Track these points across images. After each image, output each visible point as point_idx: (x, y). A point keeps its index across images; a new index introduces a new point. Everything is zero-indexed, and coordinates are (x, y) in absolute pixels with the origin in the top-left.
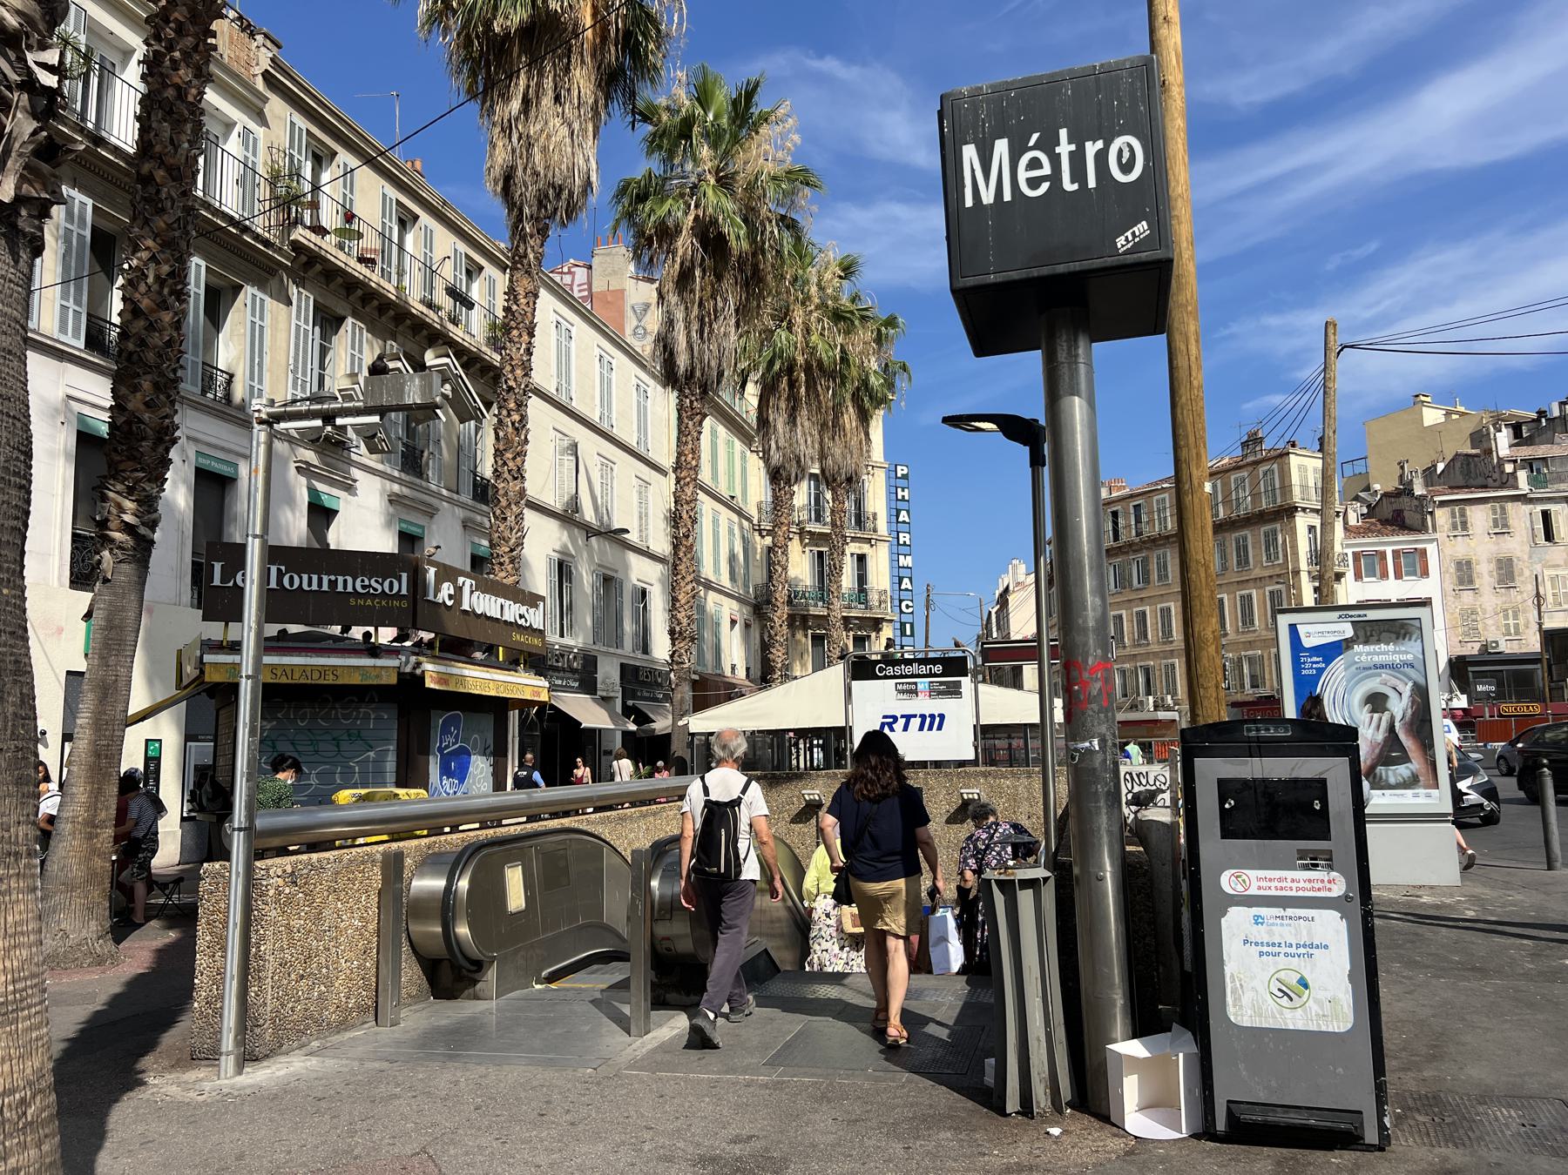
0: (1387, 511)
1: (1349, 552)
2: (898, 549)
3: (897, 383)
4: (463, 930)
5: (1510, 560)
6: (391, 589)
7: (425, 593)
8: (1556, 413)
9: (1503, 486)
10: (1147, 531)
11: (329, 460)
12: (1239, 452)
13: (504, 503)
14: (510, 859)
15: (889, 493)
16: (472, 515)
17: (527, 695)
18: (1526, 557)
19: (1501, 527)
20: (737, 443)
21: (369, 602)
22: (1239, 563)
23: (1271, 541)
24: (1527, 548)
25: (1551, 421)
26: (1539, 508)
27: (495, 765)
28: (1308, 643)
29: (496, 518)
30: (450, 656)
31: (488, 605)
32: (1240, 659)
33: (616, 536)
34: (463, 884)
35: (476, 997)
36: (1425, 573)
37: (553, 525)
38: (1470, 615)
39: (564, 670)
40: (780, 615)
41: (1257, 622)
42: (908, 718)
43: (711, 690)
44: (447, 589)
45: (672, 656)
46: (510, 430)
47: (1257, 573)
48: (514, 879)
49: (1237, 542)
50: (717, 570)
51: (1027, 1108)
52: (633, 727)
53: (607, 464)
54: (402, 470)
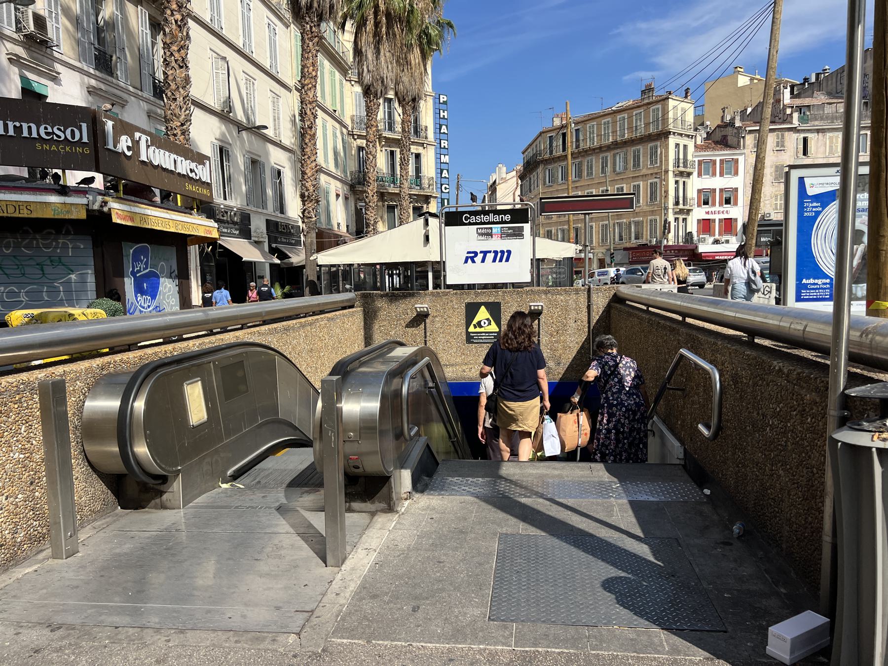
0: (718, 136)
1: (696, 160)
2: (440, 151)
3: (446, 35)
4: (142, 450)
6: (73, 136)
7: (105, 143)
8: (813, 80)
9: (784, 122)
11: (35, 55)
12: (638, 96)
13: (173, 86)
14: (189, 376)
15: (435, 113)
16: (154, 108)
17: (201, 233)
20: (337, 74)
21: (54, 148)
22: (634, 165)
23: (653, 153)
25: (811, 84)
26: (802, 135)
27: (180, 286)
28: (811, 192)
29: (168, 98)
30: (133, 198)
31: (162, 158)
32: (630, 223)
33: (257, 131)
34: (140, 405)
35: (164, 507)
36: (736, 173)
37: (214, 121)
39: (228, 222)
40: (372, 189)
41: (641, 201)
42: (485, 253)
43: (326, 240)
44: (124, 143)
45: (303, 213)
46: (174, 26)
47: (644, 171)
48: (195, 398)
49: (634, 152)
50: (326, 161)
52: (278, 261)
53: (250, 79)
54: (96, 69)
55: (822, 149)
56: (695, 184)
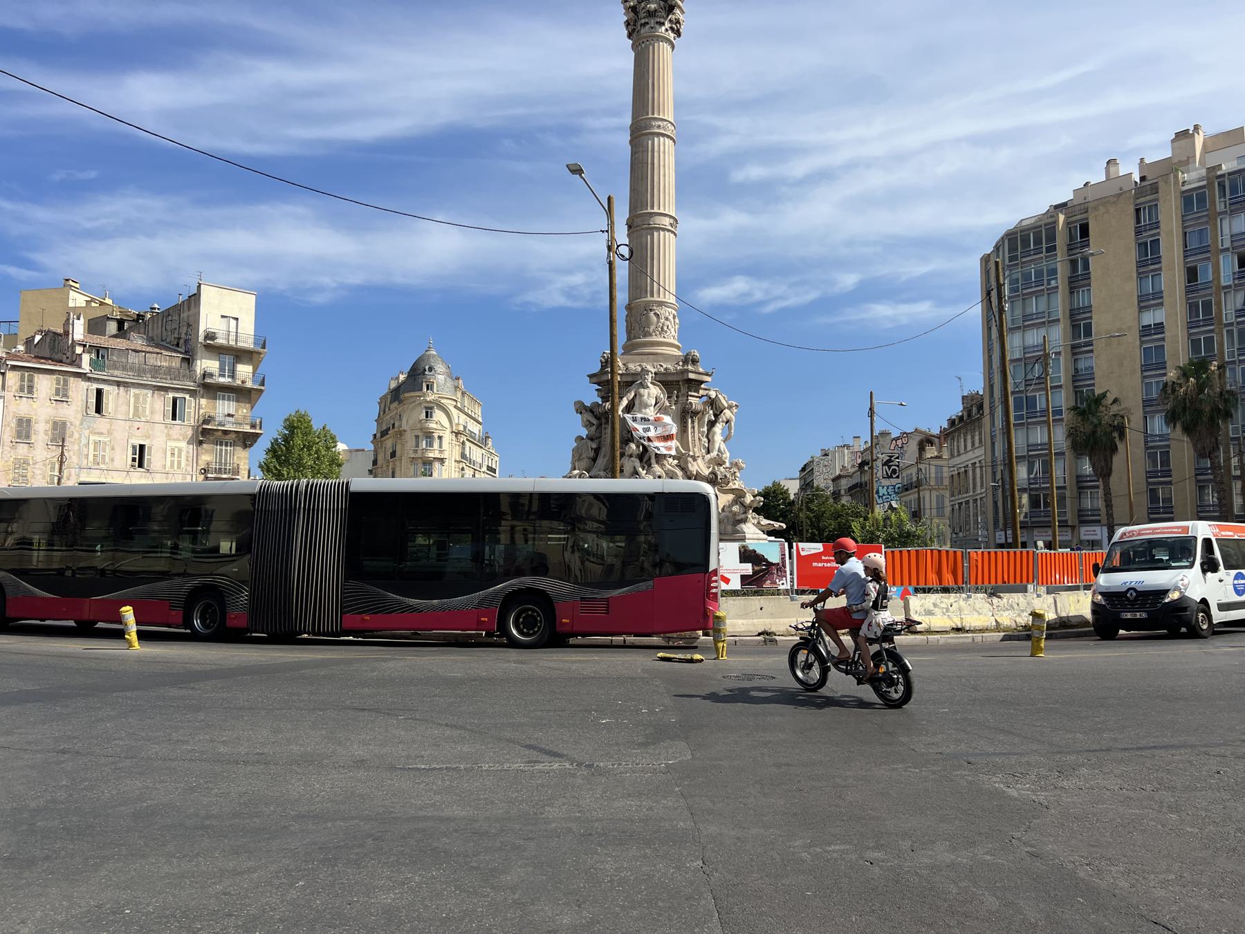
5: (64, 423)
9: (72, 364)
18: (78, 423)
19: (61, 396)
24: (80, 416)
26: (95, 386)
51: (1144, 377)
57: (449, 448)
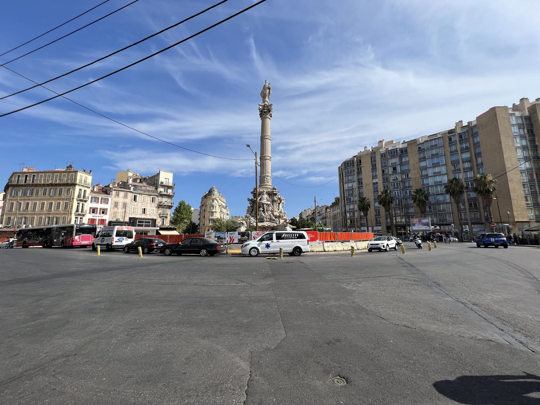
0: (104, 190)
10: (35, 182)
19: (126, 197)
23: (68, 190)
36: (107, 203)
38: (115, 213)
47: (63, 197)
55: (140, 200)
56: (88, 205)
57: (218, 209)
